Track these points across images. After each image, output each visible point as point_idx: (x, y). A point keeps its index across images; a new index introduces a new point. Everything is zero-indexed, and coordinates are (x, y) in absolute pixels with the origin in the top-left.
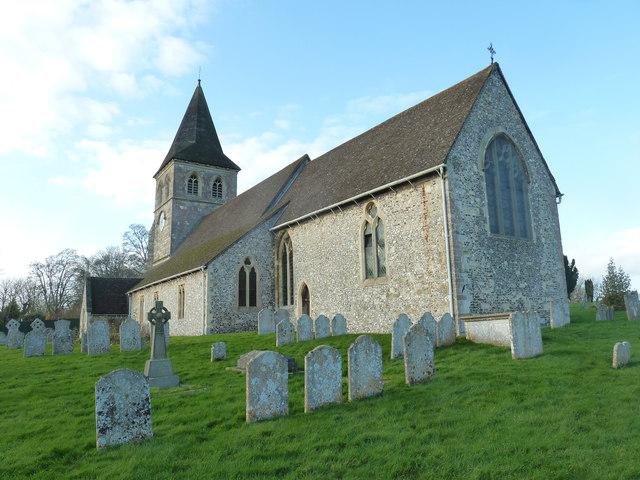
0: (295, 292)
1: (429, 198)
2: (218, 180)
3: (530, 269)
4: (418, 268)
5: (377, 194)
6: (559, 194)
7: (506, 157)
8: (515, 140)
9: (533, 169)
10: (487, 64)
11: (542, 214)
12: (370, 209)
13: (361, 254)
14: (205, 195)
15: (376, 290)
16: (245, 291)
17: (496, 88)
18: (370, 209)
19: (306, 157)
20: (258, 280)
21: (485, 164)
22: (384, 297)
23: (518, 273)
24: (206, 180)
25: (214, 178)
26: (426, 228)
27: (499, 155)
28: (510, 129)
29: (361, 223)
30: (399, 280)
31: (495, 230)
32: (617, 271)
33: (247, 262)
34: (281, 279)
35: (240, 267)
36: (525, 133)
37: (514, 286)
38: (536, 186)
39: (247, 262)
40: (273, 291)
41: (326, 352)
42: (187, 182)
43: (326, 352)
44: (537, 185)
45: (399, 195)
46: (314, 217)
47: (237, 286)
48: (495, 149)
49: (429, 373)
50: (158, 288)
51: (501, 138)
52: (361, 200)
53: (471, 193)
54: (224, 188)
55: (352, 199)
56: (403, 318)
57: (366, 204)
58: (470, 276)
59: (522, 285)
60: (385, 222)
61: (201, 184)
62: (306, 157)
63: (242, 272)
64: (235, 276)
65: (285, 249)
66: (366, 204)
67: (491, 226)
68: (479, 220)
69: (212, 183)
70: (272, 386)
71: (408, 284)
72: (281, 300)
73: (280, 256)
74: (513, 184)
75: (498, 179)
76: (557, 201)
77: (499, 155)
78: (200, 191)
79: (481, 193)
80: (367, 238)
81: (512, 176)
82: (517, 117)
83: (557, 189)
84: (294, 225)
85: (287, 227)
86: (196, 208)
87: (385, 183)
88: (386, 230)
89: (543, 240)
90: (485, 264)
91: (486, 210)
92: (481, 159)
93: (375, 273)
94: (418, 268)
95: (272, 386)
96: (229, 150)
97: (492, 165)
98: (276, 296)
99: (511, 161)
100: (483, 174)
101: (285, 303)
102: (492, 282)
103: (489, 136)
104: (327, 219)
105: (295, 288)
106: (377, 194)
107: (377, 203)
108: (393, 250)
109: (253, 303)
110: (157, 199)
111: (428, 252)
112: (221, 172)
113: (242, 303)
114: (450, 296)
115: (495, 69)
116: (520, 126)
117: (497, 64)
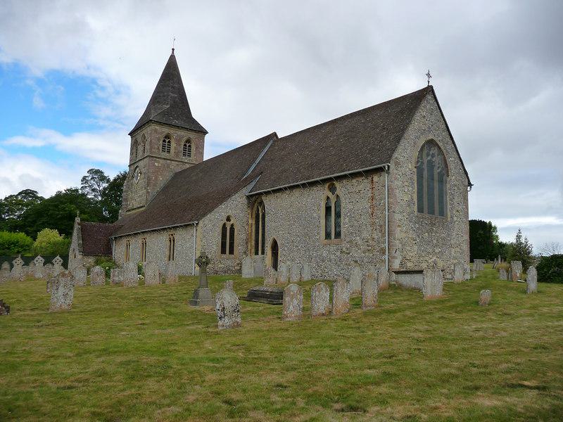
0: (266, 245)
1: (376, 185)
2: (188, 141)
3: (443, 239)
4: (365, 235)
5: (339, 178)
6: (470, 185)
7: (433, 157)
8: (440, 144)
9: (451, 166)
10: (424, 85)
11: (456, 200)
12: (332, 189)
13: (323, 221)
14: (177, 154)
15: (333, 248)
16: (226, 242)
17: (429, 97)
18: (332, 189)
19: (275, 135)
20: (236, 233)
21: (418, 162)
22: (338, 254)
23: (435, 241)
24: (178, 141)
25: (185, 139)
26: (372, 207)
27: (428, 155)
28: (439, 138)
29: (324, 198)
30: (351, 242)
31: (420, 210)
32: (523, 240)
33: (228, 219)
34: (254, 234)
35: (222, 223)
36: (449, 139)
37: (431, 251)
38: (453, 179)
39: (228, 219)
40: (247, 243)
41: (322, 286)
42: (161, 142)
43: (322, 286)
44: (454, 177)
45: (354, 181)
46: (286, 188)
47: (220, 237)
48: (425, 152)
49: (374, 301)
50: (146, 236)
51: (431, 143)
52: (324, 181)
53: (406, 184)
54: (193, 148)
55: (318, 179)
56: (98, 174)
57: (328, 184)
58: (401, 243)
59: (437, 251)
60: (342, 199)
61: (173, 145)
62: (275, 135)
63: (224, 227)
64: (219, 230)
65: (258, 210)
66: (328, 184)
67: (418, 208)
68: (409, 204)
69: (183, 144)
70: (295, 302)
71: (356, 245)
72: (253, 250)
73: (254, 216)
74: (436, 177)
75: (425, 173)
76: (469, 189)
77: (428, 155)
78: (172, 151)
79: (413, 184)
80: (328, 209)
81: (436, 171)
82: (444, 126)
83: (469, 181)
84: (267, 193)
85: (261, 194)
86: (168, 167)
87: (343, 171)
88: (343, 205)
89: (455, 219)
90: (412, 235)
91: (415, 196)
92: (414, 160)
93: (333, 236)
94: (365, 235)
95: (295, 302)
96: (196, 114)
97: (422, 163)
98: (249, 247)
99: (437, 160)
100: (415, 170)
101: (257, 253)
102: (416, 247)
103: (421, 142)
104: (297, 192)
105: (266, 242)
106: (339, 178)
107: (337, 185)
108: (347, 220)
109: (231, 252)
110: (131, 154)
111: (373, 224)
112: (192, 135)
113: (223, 251)
114: (387, 256)
115: (429, 90)
116: (445, 133)
117: (432, 87)
